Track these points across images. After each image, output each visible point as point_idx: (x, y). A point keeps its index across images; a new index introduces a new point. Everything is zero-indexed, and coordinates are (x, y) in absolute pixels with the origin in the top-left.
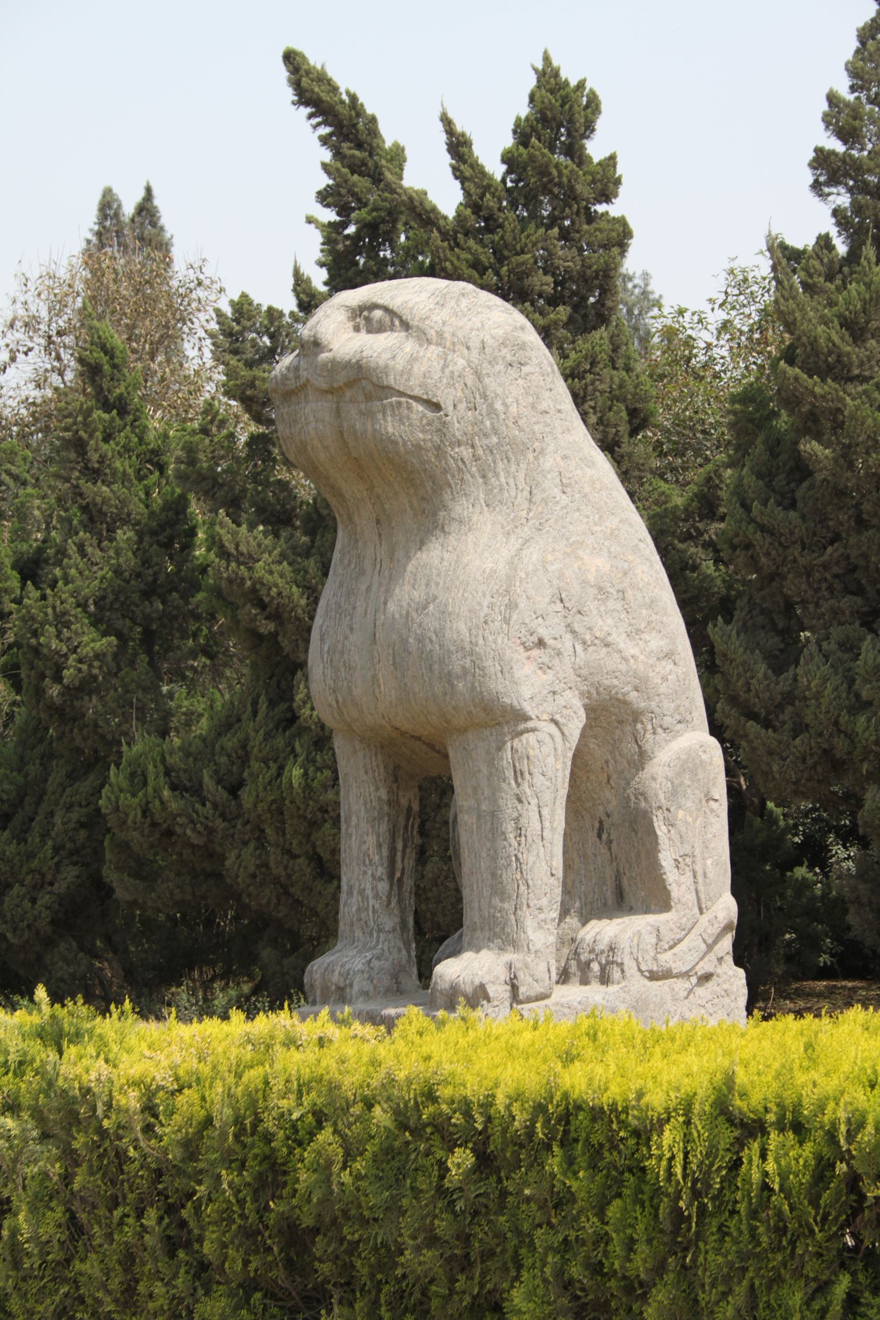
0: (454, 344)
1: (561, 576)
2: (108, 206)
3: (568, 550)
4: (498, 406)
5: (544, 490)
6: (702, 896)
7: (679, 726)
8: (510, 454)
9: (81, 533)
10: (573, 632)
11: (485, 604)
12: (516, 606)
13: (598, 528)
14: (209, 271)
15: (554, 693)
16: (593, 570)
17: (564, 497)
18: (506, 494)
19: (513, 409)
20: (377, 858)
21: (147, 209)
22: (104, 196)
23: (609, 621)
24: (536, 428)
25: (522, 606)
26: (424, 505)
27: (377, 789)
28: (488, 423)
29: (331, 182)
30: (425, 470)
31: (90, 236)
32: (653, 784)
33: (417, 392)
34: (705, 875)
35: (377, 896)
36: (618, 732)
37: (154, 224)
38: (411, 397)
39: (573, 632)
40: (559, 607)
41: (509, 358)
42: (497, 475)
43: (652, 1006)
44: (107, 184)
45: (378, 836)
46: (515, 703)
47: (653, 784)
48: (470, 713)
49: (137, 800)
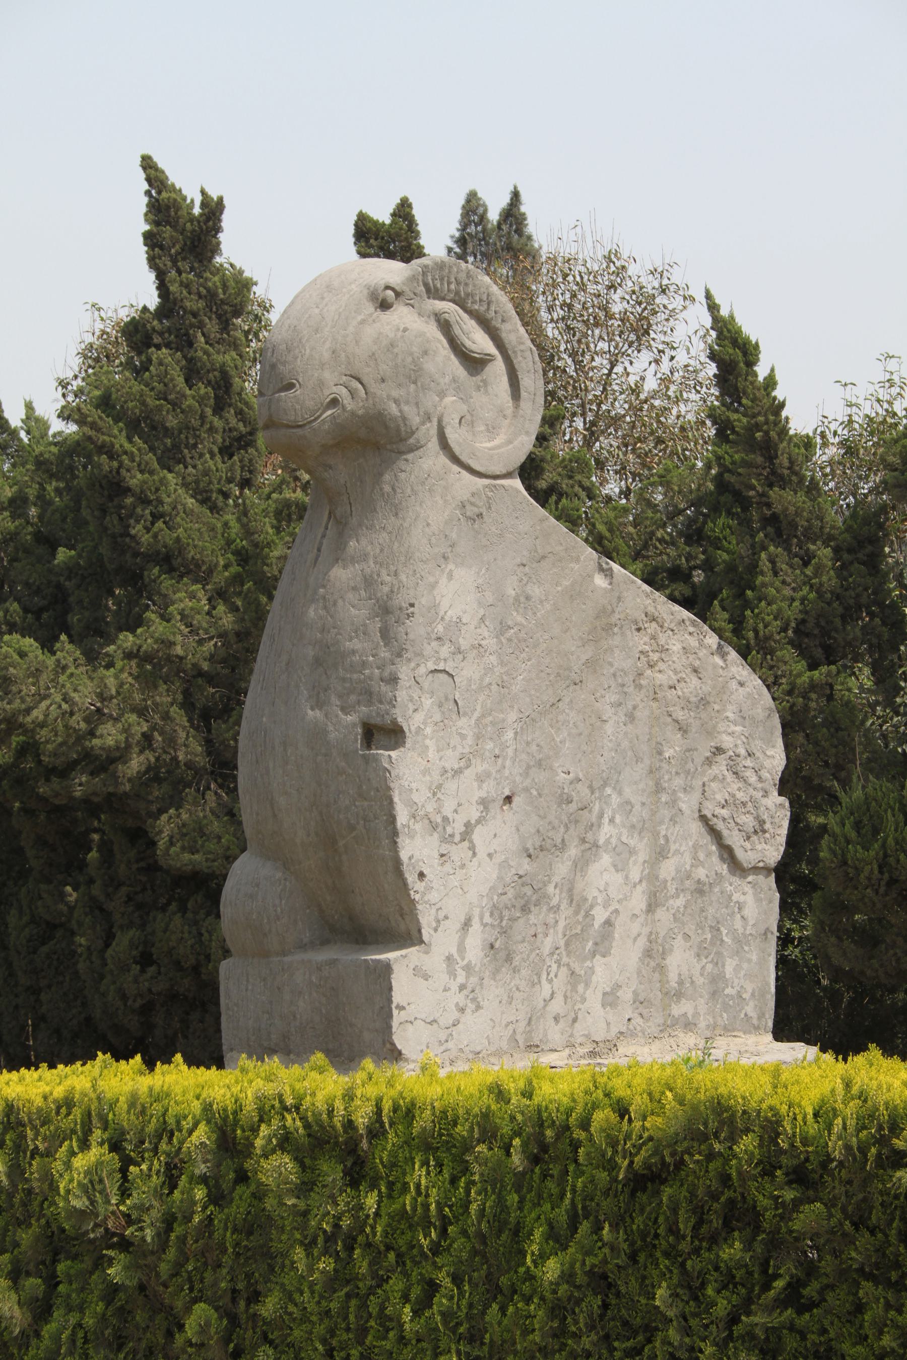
2: (472, 208)
9: (772, 548)
14: (677, 277)
21: (513, 214)
22: (468, 201)
31: (451, 244)
32: (419, 886)
34: (692, 982)
37: (519, 231)
44: (472, 188)
47: (419, 886)
49: (872, 853)
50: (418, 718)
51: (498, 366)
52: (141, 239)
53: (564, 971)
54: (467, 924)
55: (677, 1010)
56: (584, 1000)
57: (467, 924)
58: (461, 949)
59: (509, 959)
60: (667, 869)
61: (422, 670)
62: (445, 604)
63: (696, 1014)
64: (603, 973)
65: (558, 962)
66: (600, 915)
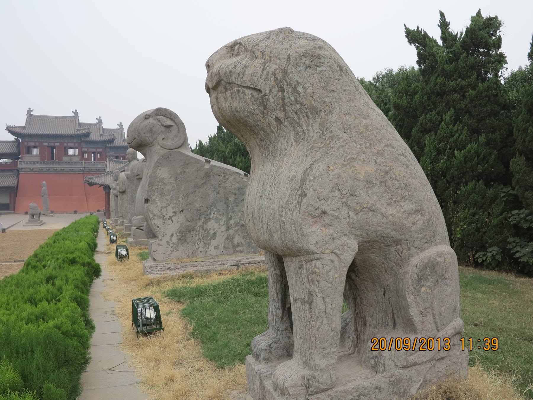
0: (270, 57)
1: (339, 177)
3: (345, 163)
4: (300, 89)
5: (331, 132)
6: (439, 324)
7: (426, 245)
8: (309, 114)
10: (347, 205)
11: (288, 194)
12: (306, 195)
13: (369, 150)
15: (333, 238)
16: (363, 172)
17: (345, 135)
18: (307, 135)
19: (310, 90)
20: (276, 299)
23: (375, 198)
24: (326, 99)
25: (309, 195)
26: (263, 143)
27: (275, 270)
28: (293, 98)
29: (417, 67)
30: (258, 125)
33: (248, 84)
35: (276, 315)
36: (387, 250)
38: (244, 87)
39: (347, 205)
40: (337, 193)
41: (308, 63)
42: (300, 126)
43: (404, 381)
45: (276, 290)
46: (305, 246)
48: (282, 250)
50: (154, 197)
51: (175, 127)
52: (492, 16)
53: (202, 243)
54: (172, 235)
55: (237, 249)
56: (208, 248)
57: (172, 235)
58: (171, 240)
59: (186, 241)
60: (232, 222)
61: (154, 188)
62: (159, 175)
63: (243, 250)
64: (214, 243)
65: (200, 241)
66: (212, 232)
